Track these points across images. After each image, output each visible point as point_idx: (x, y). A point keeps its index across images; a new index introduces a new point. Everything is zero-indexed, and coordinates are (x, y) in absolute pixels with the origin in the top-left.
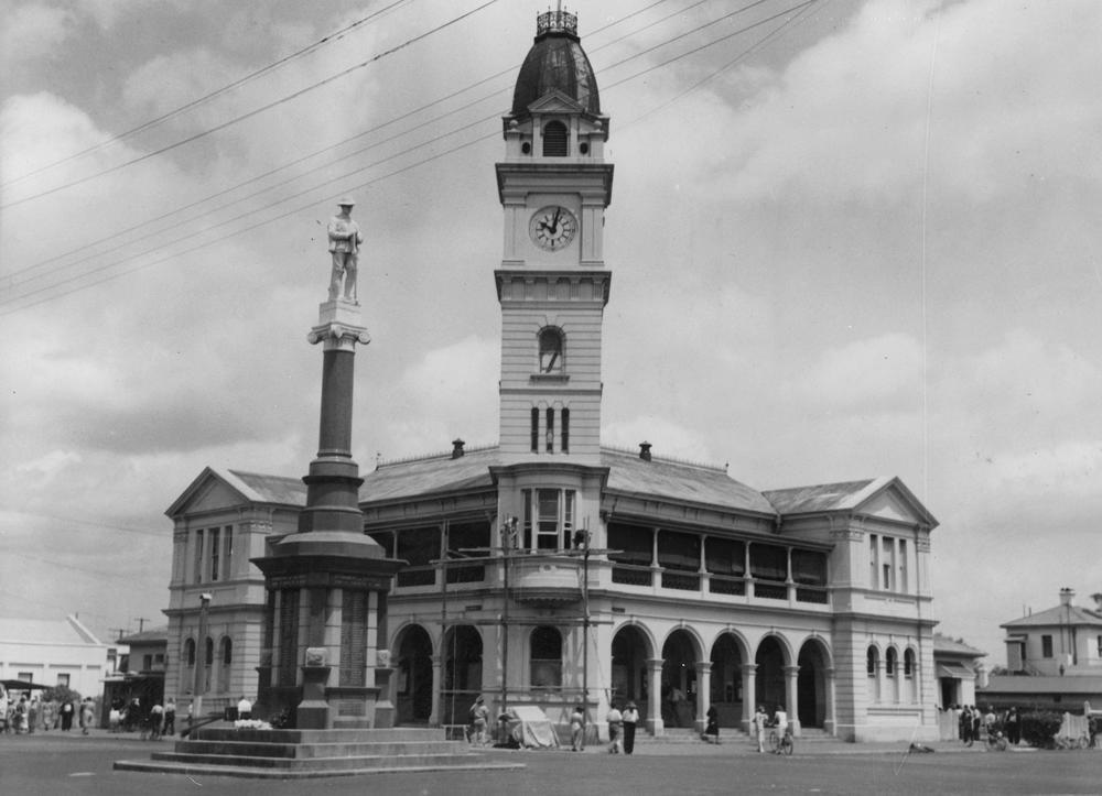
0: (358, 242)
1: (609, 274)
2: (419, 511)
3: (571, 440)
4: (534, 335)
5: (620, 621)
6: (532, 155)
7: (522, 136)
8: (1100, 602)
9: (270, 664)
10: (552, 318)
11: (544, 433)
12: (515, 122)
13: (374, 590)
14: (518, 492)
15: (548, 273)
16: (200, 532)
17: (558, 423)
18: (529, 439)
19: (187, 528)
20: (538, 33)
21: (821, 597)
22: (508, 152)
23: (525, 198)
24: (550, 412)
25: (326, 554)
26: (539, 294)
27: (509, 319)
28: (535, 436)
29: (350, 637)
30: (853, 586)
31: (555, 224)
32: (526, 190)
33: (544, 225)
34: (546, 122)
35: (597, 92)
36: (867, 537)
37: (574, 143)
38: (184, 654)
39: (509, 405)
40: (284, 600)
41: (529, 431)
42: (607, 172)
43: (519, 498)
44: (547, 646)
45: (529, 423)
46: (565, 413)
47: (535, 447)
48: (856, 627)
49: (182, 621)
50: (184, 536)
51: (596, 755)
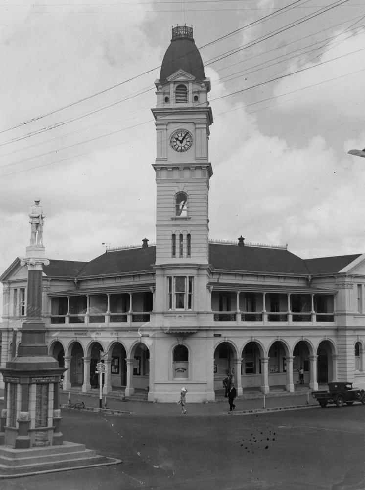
0: (42, 218)
3: (192, 250)
4: (172, 197)
5: (219, 341)
6: (170, 103)
7: (164, 93)
9: (6, 416)
11: (179, 243)
12: (161, 86)
13: (52, 382)
14: (166, 278)
15: (178, 164)
16: (16, 290)
17: (185, 241)
18: (171, 250)
19: (9, 288)
20: (173, 38)
21: (331, 319)
23: (167, 125)
24: (181, 236)
26: (176, 175)
27: (160, 189)
28: (174, 247)
29: (41, 405)
30: (347, 312)
31: (183, 139)
32: (168, 121)
33: (177, 139)
34: (176, 85)
36: (355, 286)
37: (190, 97)
38: (10, 350)
40: (11, 388)
41: (171, 246)
43: (167, 282)
44: (181, 354)
46: (189, 236)
48: (348, 333)
49: (8, 334)
50: (8, 291)
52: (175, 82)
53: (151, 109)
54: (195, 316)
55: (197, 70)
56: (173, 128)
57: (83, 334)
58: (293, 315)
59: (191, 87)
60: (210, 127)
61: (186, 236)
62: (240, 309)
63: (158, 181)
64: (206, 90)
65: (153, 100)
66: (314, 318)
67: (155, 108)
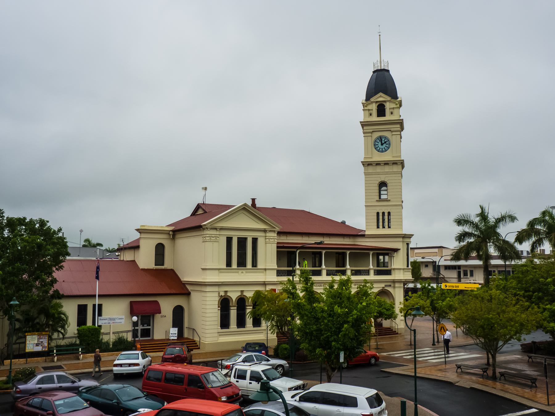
1: (403, 160)
10: (383, 178)
17: (386, 217)
21: (388, 272)
22: (363, 135)
24: (383, 213)
25: (522, 402)
26: (379, 169)
32: (372, 130)
34: (377, 104)
35: (379, 189)
37: (388, 112)
42: (401, 123)
45: (376, 217)
46: (389, 213)
47: (378, 227)
52: (377, 101)
53: (360, 122)
55: (392, 92)
57: (320, 285)
58: (327, 270)
59: (388, 106)
60: (402, 133)
61: (387, 213)
63: (366, 174)
66: (324, 272)
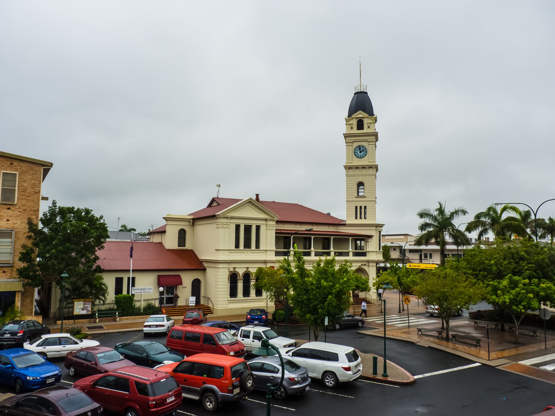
1: (377, 165)
2: (465, 329)
8: (1, 332)
10: (361, 179)
21: (364, 254)
24: (361, 207)
26: (357, 172)
32: (353, 141)
34: (357, 120)
37: (365, 126)
39: (349, 180)
46: (365, 207)
47: (356, 218)
51: (510, 366)
54: (264, 253)
55: (370, 111)
56: (356, 144)
58: (315, 252)
59: (366, 121)
61: (364, 207)
62: (313, 248)
64: (375, 122)
65: (344, 129)
67: (345, 133)
